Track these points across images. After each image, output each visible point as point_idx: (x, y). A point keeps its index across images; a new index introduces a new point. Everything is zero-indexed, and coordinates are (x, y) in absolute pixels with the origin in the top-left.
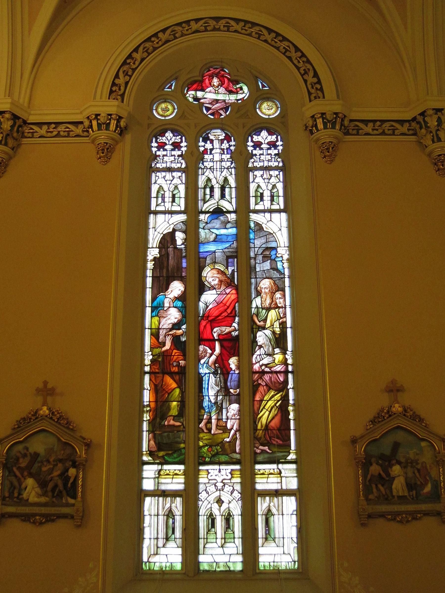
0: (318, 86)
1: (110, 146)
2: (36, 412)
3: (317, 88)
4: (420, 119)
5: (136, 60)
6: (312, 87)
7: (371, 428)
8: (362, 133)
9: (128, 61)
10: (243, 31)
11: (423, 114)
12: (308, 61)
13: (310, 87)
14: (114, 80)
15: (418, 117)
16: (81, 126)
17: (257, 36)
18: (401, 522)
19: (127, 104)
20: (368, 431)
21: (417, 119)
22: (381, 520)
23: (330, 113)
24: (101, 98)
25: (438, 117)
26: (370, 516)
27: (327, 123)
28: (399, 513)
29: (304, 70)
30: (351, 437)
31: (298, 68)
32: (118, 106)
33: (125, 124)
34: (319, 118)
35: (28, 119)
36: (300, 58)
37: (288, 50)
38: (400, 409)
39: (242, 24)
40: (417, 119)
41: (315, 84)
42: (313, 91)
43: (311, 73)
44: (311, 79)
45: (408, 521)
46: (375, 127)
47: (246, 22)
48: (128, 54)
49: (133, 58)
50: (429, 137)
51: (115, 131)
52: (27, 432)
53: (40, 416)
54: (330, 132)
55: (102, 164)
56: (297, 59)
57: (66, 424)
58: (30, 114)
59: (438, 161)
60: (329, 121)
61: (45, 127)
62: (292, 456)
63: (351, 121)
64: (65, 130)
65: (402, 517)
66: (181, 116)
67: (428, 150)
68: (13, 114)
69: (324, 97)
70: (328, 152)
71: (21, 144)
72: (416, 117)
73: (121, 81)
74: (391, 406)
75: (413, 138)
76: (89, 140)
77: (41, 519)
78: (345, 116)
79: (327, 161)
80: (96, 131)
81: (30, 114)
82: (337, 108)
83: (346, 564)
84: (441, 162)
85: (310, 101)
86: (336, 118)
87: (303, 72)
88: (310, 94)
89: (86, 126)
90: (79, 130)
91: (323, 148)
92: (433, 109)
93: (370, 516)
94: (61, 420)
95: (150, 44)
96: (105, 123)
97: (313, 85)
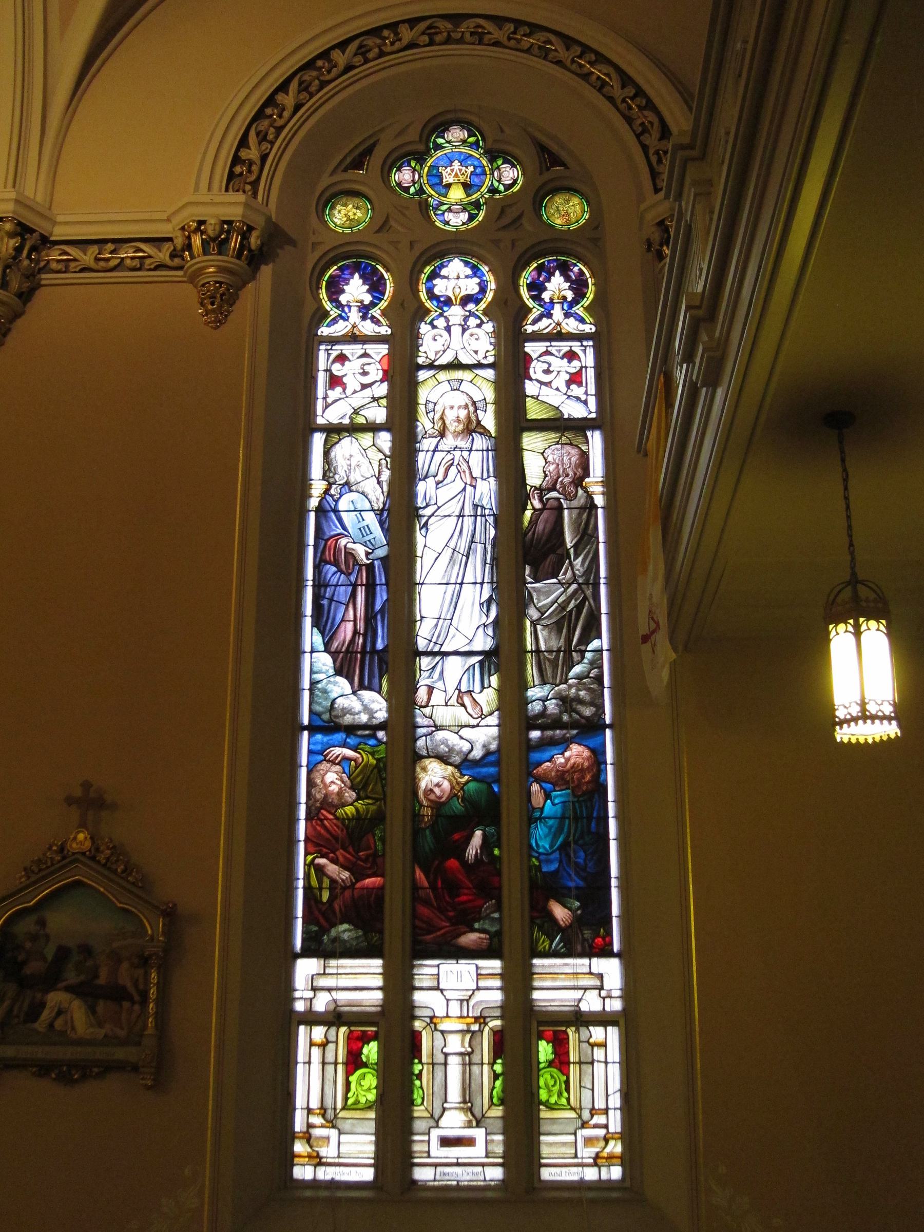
2: (62, 849)
5: (283, 110)
9: (320, 63)
16: (167, 248)
19: (265, 202)
24: (209, 189)
31: (629, 120)
33: (259, 242)
35: (51, 234)
36: (632, 99)
47: (518, 23)
49: (276, 105)
53: (70, 853)
55: (212, 327)
58: (55, 223)
61: (93, 250)
66: (381, 226)
68: (20, 224)
71: (39, 286)
79: (209, 322)
80: (199, 256)
81: (55, 223)
86: (228, 232)
89: (179, 247)
90: (163, 255)
91: (203, 294)
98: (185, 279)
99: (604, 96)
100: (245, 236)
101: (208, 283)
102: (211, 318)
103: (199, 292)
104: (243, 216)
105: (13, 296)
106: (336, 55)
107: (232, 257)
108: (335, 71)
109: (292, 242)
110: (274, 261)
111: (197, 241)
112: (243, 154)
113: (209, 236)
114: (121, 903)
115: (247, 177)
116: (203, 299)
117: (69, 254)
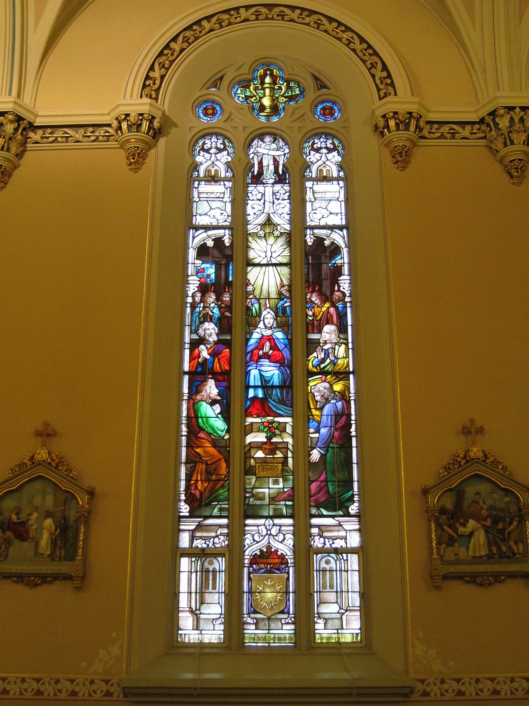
0: (389, 81)
1: (142, 151)
2: (32, 458)
3: (387, 83)
4: (489, 120)
6: (382, 83)
7: (444, 476)
8: (459, 137)
9: (166, 52)
10: (300, 20)
11: (493, 114)
12: (375, 53)
13: (378, 82)
14: (148, 72)
15: (487, 118)
17: (316, 26)
18: (481, 585)
20: (442, 480)
21: (485, 120)
22: (458, 582)
23: (404, 112)
25: (511, 117)
26: (445, 577)
27: (399, 124)
28: (481, 575)
29: (371, 63)
30: (421, 486)
31: (364, 62)
32: (151, 104)
33: (158, 125)
34: (391, 118)
35: (35, 122)
36: (365, 50)
37: (352, 42)
38: (481, 454)
39: (298, 12)
40: (485, 120)
41: (384, 78)
42: (381, 86)
43: (379, 66)
44: (379, 74)
45: (490, 584)
46: (473, 130)
48: (165, 44)
49: (201, 26)
50: (500, 140)
51: (148, 134)
52: (509, 485)
54: (403, 134)
56: (362, 51)
57: (66, 471)
59: (511, 167)
60: (402, 122)
62: (354, 509)
63: (428, 122)
64: (62, 135)
65: (483, 579)
67: (499, 155)
68: (17, 116)
69: (396, 95)
70: (401, 157)
72: (484, 117)
73: (156, 74)
74: (469, 450)
75: (483, 142)
76: (118, 144)
77: (36, 580)
78: (421, 117)
80: (393, 132)
81: (37, 116)
82: (414, 108)
83: (421, 635)
84: (515, 168)
85: (380, 99)
87: (369, 66)
88: (379, 90)
91: (128, 154)
92: (505, 107)
93: (445, 577)
94: (60, 466)
95: (192, 32)
96: (404, 121)
97: (383, 79)
98: (118, 146)
99: (350, 48)
100: (151, 121)
101: (131, 147)
102: (132, 167)
103: (126, 153)
104: (149, 111)
105: (13, 156)
106: (204, 23)
107: (144, 133)
108: (175, 54)
109: (176, 126)
110: (167, 136)
111: (124, 125)
112: (151, 74)
113: (131, 122)
114: (65, 487)
115: (152, 87)
116: (128, 157)
117: (68, 133)
